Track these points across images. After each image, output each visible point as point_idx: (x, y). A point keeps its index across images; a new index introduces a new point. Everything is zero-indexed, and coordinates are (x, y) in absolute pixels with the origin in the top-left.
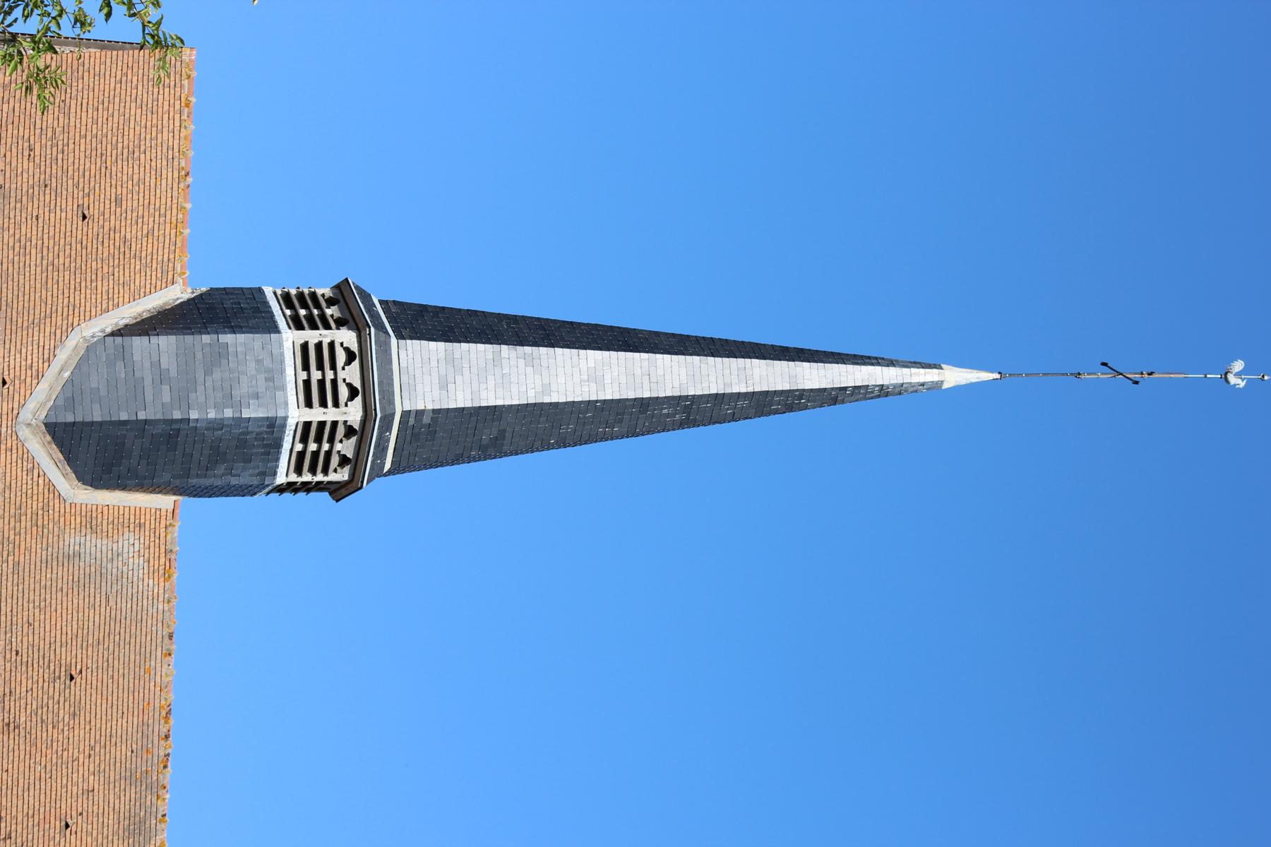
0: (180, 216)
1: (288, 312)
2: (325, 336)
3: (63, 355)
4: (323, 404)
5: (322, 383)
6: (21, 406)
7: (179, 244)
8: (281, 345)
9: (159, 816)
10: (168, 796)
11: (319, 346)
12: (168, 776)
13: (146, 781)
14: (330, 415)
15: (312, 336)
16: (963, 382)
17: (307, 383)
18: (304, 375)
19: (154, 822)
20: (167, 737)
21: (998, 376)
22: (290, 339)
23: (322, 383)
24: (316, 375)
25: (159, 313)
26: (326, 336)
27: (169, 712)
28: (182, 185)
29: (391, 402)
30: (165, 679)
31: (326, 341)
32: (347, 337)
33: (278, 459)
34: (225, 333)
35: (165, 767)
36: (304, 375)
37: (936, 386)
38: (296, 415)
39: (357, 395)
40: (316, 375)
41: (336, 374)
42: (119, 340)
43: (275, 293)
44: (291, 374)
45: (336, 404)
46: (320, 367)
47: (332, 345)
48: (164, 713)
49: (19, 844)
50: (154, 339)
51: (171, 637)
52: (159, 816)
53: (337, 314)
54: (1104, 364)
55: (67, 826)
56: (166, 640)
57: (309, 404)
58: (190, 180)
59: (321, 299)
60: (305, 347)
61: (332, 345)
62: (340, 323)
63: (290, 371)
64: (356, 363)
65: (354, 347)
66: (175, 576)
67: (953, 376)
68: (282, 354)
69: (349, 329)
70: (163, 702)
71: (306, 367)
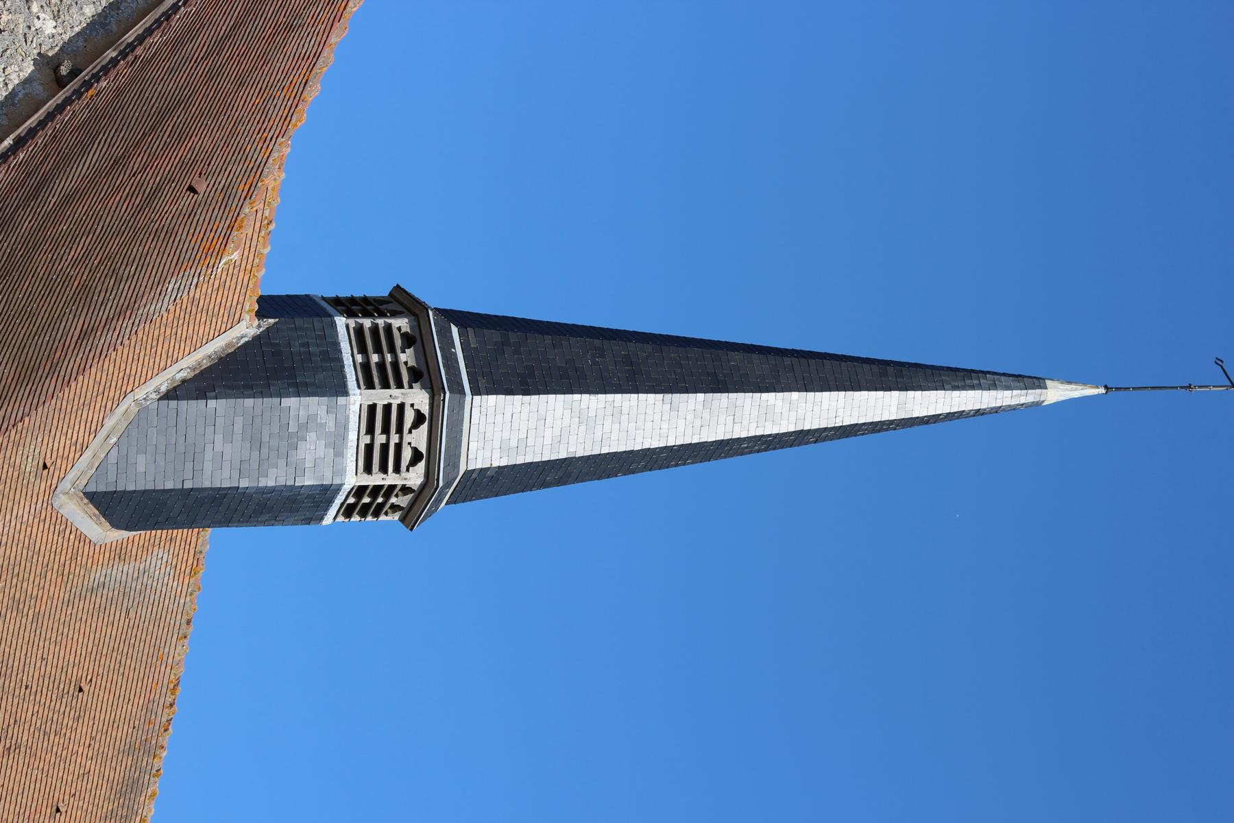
0: (257, 260)
1: (359, 358)
2: (394, 396)
3: (109, 423)
4: (384, 469)
5: (385, 448)
6: (60, 480)
7: (251, 286)
8: (346, 407)
9: (154, 771)
10: (164, 754)
11: (387, 408)
12: (165, 740)
13: (144, 749)
14: (391, 479)
15: (381, 397)
16: (1063, 398)
17: (369, 448)
18: (366, 439)
19: (147, 777)
20: (171, 705)
21: (1102, 391)
22: (357, 399)
23: (385, 448)
24: (380, 439)
25: (221, 359)
26: (396, 398)
27: (177, 685)
28: (263, 233)
29: (456, 465)
30: (177, 658)
31: (395, 403)
32: (419, 398)
33: (327, 510)
34: (288, 396)
35: (166, 730)
36: (366, 439)
37: (1037, 404)
38: (352, 480)
39: (420, 460)
40: (375, 358)
41: (401, 438)
42: (173, 403)
43: (347, 326)
44: (354, 437)
45: (397, 469)
46: (386, 430)
47: (401, 407)
48: (171, 686)
49: (10, 820)
50: (212, 403)
51: (189, 622)
52: (154, 771)
53: (412, 363)
54: (1219, 362)
55: (58, 810)
56: (184, 626)
57: (368, 469)
58: (272, 227)
59: (396, 332)
60: (372, 408)
61: (401, 407)
62: (416, 375)
63: (352, 436)
64: (424, 428)
65: (425, 410)
66: (200, 575)
67: (1055, 393)
68: (347, 419)
69: (423, 387)
70: (172, 677)
71: (370, 430)
